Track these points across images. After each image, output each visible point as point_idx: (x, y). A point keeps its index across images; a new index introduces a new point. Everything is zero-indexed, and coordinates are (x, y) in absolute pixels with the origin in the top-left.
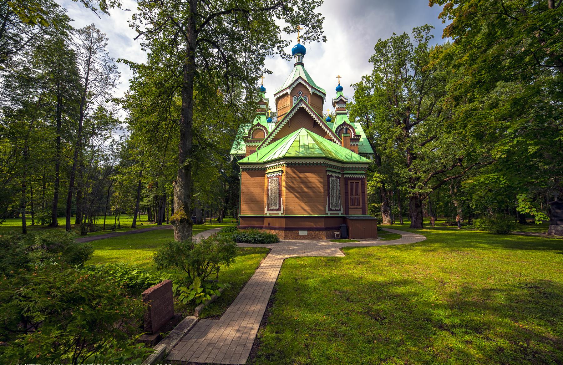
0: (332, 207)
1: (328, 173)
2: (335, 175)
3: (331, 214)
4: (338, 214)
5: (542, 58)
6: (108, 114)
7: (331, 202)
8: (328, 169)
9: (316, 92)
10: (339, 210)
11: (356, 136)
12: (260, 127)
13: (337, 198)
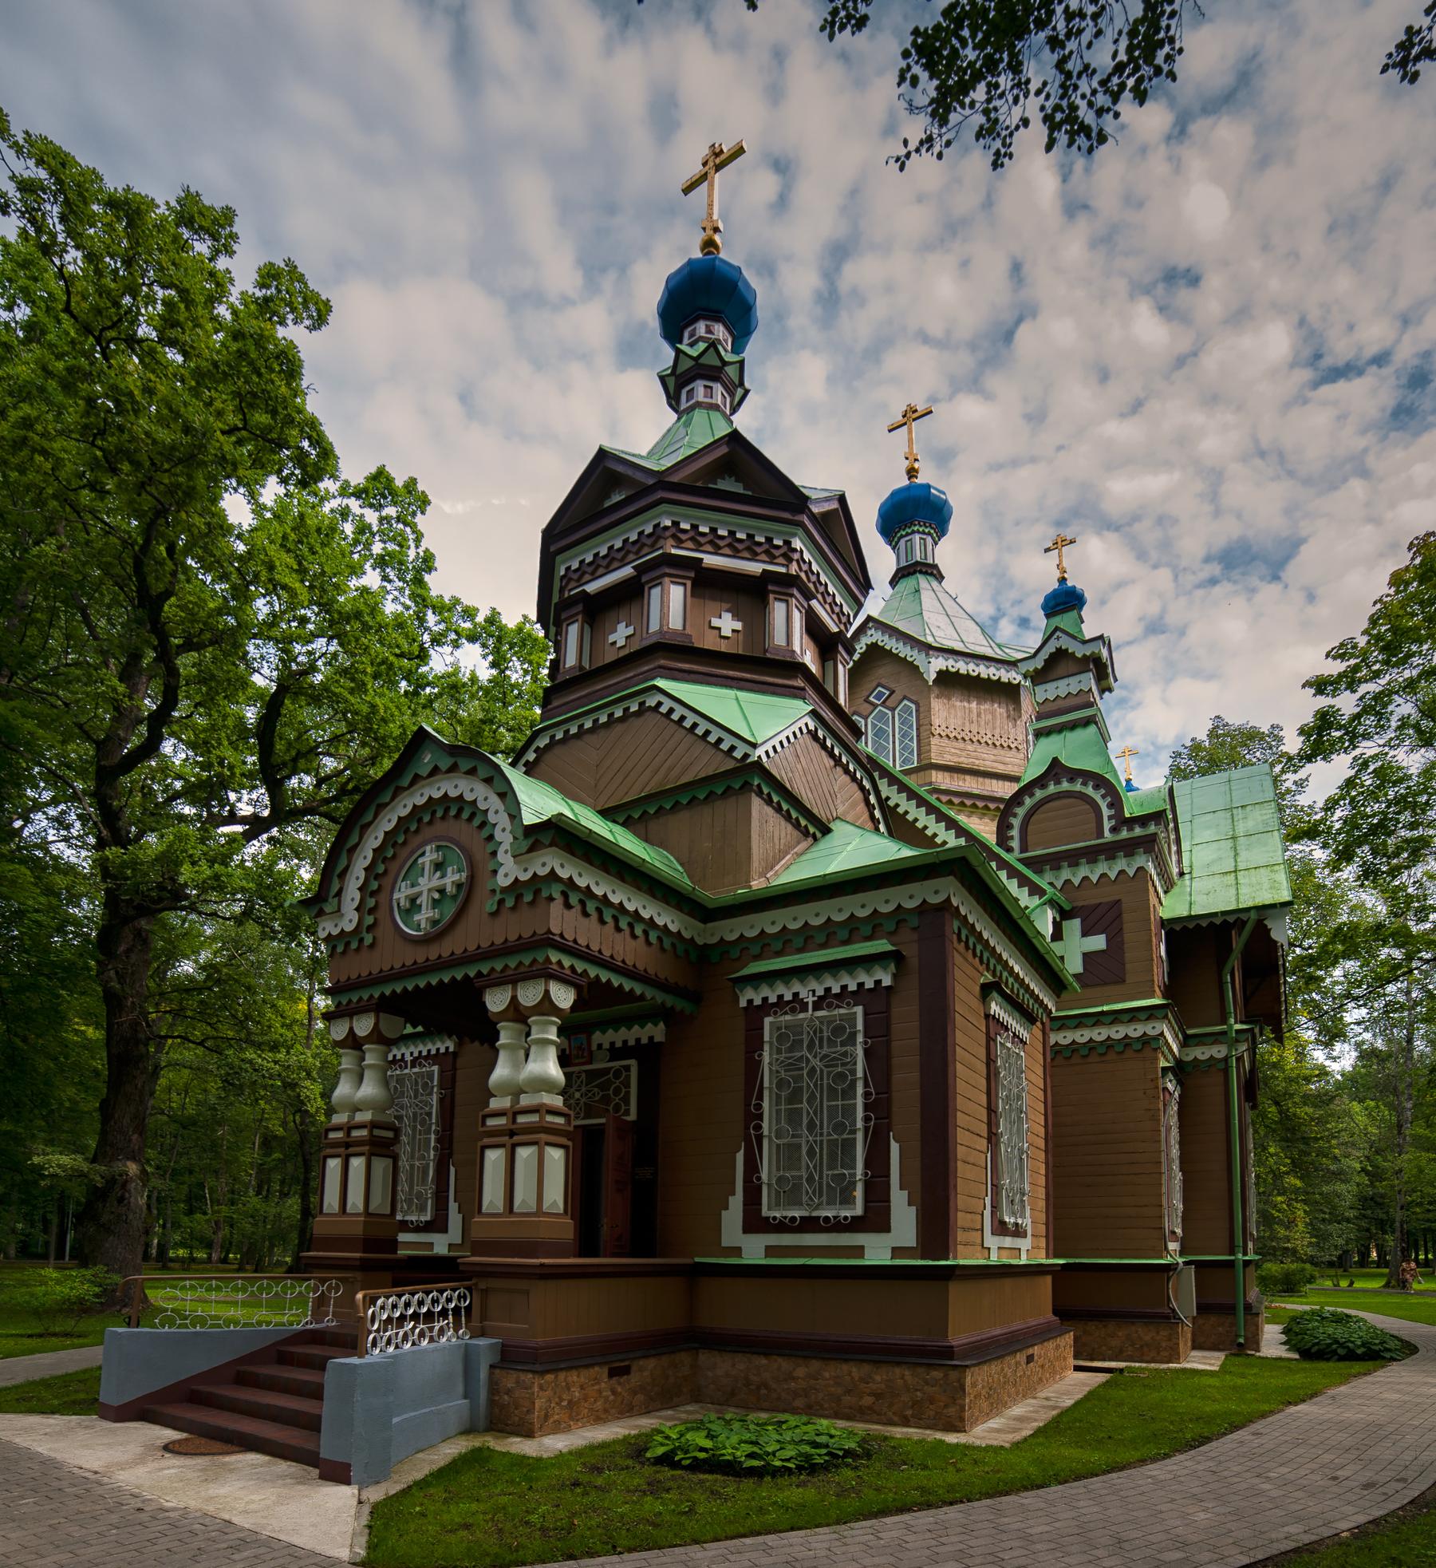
2: (808, 990)
3: (770, 1251)
9: (963, 667)
11: (1132, 822)
12: (1065, 786)
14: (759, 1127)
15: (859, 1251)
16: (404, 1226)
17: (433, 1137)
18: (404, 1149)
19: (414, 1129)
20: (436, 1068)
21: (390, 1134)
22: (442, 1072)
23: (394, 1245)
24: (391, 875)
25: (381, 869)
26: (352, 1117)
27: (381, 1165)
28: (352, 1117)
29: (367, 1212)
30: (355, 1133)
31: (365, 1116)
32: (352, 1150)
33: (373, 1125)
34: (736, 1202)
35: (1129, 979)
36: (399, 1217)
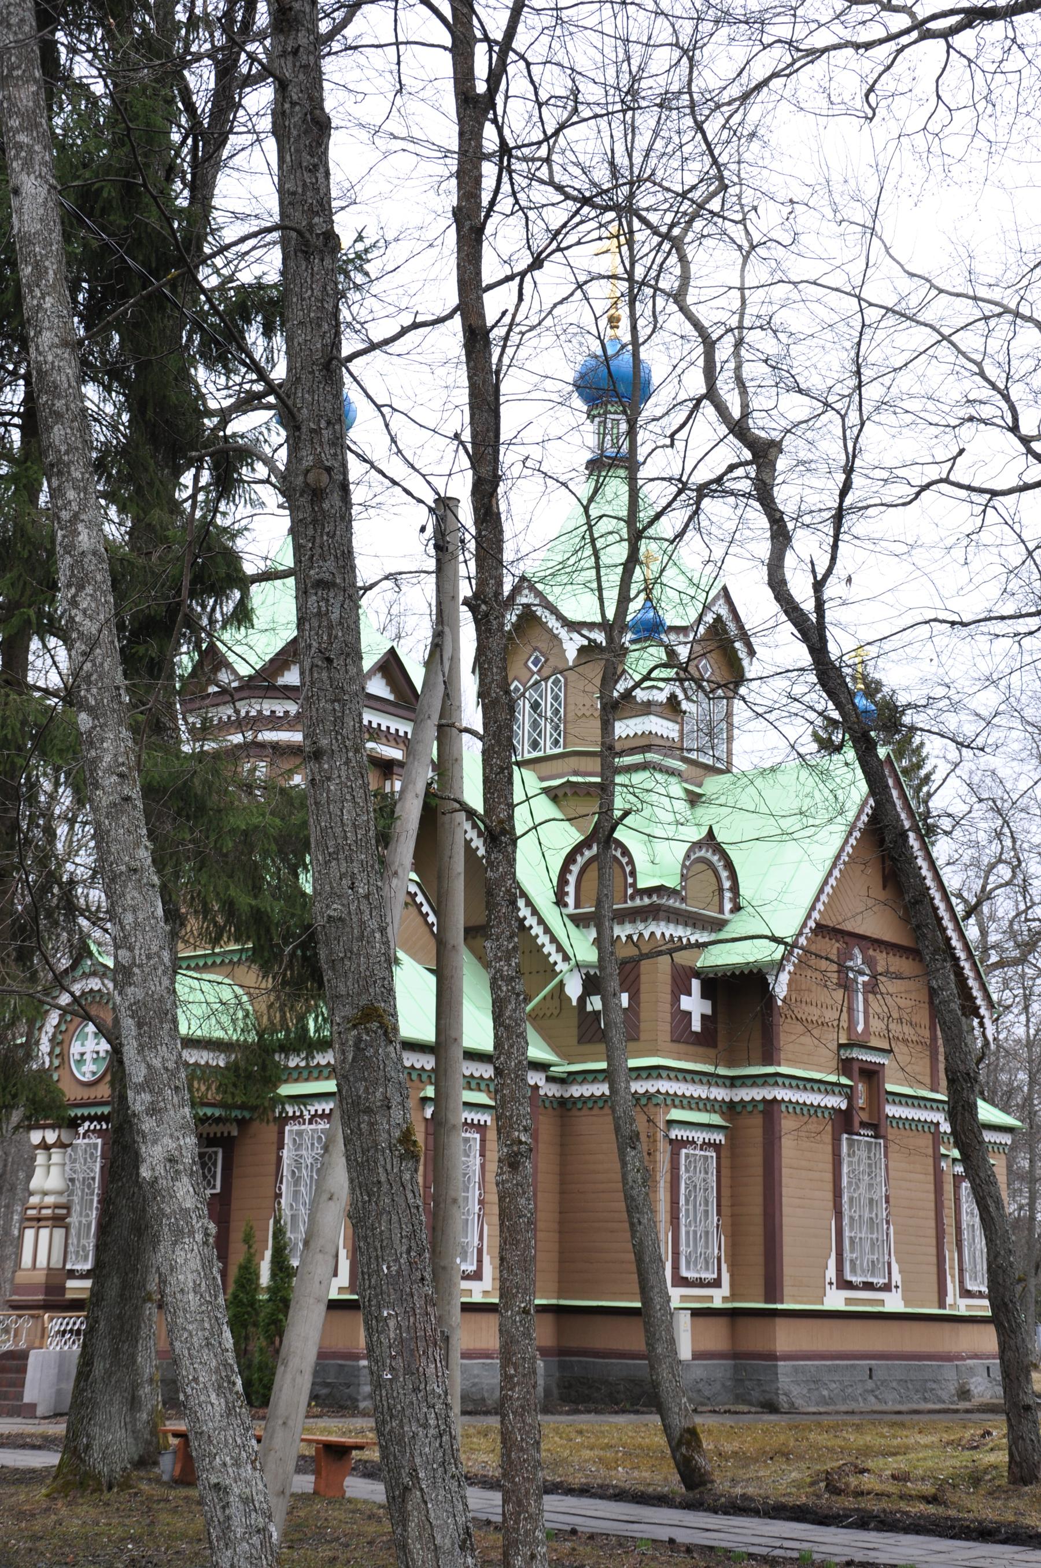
0: (688, 1268)
1: (675, 1133)
2: (700, 1136)
3: (848, 1301)
4: (882, 1302)
5: (13, 904)
6: (593, 362)
7: (683, 1248)
8: (676, 1114)
10: (717, 1283)
13: (707, 1233)
14: (279, 1203)
15: (848, 1301)
16: (72, 1274)
17: (96, 1199)
18: (73, 1220)
19: (83, 1190)
20: (99, 1141)
21: (64, 1211)
22: (103, 1145)
23: (63, 1289)
24: (70, 1032)
25: (63, 1028)
26: (42, 1200)
27: (59, 1233)
28: (42, 1200)
29: (49, 1268)
30: (44, 1212)
31: (50, 1200)
32: (42, 1223)
33: (56, 1206)
34: (268, 1254)
35: (643, 1036)
36: (68, 1267)
